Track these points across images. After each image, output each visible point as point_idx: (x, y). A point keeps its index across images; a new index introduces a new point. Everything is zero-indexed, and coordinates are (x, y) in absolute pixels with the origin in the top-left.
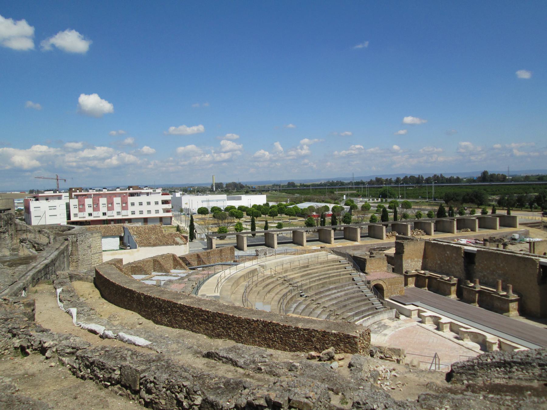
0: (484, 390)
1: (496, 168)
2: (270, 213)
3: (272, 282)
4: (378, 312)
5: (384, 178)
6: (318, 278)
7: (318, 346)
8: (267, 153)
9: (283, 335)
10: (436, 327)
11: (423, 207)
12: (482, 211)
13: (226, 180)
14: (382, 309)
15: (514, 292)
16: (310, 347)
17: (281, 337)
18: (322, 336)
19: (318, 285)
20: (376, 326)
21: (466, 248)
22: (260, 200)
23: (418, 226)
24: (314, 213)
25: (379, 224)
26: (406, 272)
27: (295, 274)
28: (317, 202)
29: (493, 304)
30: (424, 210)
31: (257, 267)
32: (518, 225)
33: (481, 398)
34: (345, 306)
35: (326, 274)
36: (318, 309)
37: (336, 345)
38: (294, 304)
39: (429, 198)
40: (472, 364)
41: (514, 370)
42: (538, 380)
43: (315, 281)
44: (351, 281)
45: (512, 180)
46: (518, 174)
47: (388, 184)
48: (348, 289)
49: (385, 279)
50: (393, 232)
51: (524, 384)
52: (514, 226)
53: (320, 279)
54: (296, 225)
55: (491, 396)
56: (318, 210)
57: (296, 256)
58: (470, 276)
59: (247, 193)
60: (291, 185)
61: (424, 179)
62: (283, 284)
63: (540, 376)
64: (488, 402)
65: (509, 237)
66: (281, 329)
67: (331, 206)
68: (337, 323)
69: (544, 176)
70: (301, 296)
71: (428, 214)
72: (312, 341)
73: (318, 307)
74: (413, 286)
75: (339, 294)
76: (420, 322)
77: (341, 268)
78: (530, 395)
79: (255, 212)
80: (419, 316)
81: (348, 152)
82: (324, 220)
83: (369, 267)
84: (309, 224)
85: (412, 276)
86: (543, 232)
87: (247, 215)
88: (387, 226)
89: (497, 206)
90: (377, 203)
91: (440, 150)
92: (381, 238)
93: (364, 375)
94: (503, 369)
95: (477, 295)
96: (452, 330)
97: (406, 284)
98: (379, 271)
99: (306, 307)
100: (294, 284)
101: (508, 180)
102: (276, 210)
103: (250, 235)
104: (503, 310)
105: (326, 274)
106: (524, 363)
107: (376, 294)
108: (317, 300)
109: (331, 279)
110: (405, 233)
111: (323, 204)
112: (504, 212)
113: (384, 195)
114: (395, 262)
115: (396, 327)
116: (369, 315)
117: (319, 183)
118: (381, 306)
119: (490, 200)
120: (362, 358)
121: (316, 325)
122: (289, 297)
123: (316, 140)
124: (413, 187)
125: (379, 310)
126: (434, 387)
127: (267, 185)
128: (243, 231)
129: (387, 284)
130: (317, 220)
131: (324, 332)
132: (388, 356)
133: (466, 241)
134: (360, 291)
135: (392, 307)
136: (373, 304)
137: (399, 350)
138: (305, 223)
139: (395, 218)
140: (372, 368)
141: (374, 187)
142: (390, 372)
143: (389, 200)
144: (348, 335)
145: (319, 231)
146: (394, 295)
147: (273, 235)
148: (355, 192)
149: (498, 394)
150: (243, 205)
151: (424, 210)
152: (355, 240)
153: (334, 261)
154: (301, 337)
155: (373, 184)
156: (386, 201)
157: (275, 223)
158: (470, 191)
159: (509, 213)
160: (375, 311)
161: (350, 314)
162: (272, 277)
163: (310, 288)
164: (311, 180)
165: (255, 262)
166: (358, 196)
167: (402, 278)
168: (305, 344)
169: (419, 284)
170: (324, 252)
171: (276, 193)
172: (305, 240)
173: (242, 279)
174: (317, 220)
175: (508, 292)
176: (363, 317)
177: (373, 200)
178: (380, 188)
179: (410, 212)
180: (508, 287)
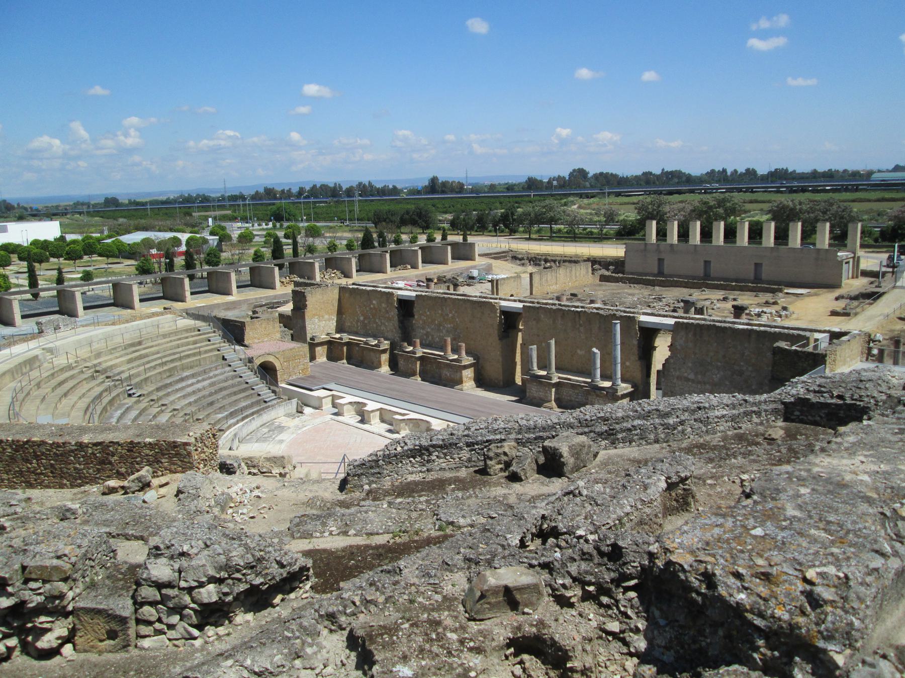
0: (390, 495)
1: (449, 173)
2: (67, 254)
3: (72, 377)
4: (269, 407)
5: (279, 189)
6: (159, 361)
7: (123, 470)
8: (57, 142)
9: (56, 461)
10: (360, 418)
11: (339, 235)
12: (428, 236)
14: (275, 402)
15: (468, 353)
16: (108, 473)
17: (52, 465)
18: (128, 451)
19: (160, 373)
20: (266, 430)
21: (400, 292)
22: (48, 231)
23: (331, 263)
24: (154, 251)
25: (268, 263)
26: (312, 339)
27: (117, 358)
28: (160, 231)
29: (439, 375)
30: (341, 238)
31: (37, 352)
32: (477, 256)
33: (385, 506)
34: (212, 404)
35: (174, 354)
36: (162, 415)
37: (155, 462)
38: (116, 410)
39: (350, 220)
40: (375, 458)
41: (434, 458)
42: (467, 467)
43: (154, 368)
44: (221, 362)
45: (472, 191)
46: (481, 182)
47: (285, 199)
48: (215, 376)
49: (278, 353)
50: (292, 276)
51: (448, 475)
52: (471, 258)
54: (120, 274)
55: (399, 500)
56: (160, 245)
57: (117, 327)
58: (407, 336)
59: (21, 218)
60: (111, 202)
62: (93, 378)
63: (469, 460)
64: (394, 511)
65: (465, 275)
66: (49, 450)
67: (184, 237)
68: (157, 426)
69: (515, 185)
70: (130, 395)
71: (347, 245)
72: (110, 463)
73: (162, 411)
74: (325, 359)
75: (199, 386)
76: (335, 414)
77: (201, 341)
78: (453, 490)
79: (35, 254)
80: (334, 405)
81: (211, 143)
82: (172, 261)
83: (250, 335)
84: (144, 270)
85: (321, 344)
86: (511, 265)
87: (21, 259)
88: (281, 267)
89: (449, 230)
90: (267, 229)
91: (366, 141)
92: (273, 287)
93: (203, 505)
94: (418, 459)
95: (418, 363)
96: (383, 420)
97: (313, 358)
98: (267, 341)
99: (140, 414)
100: (114, 376)
101: (467, 191)
102: (79, 248)
103: (29, 296)
104: (454, 382)
105: (174, 354)
106: (447, 446)
107: (263, 378)
108: (160, 399)
109: (184, 361)
110: (312, 277)
111: (169, 235)
112: (459, 239)
113: (278, 217)
114: (294, 324)
115: (297, 427)
116: (253, 414)
117: (164, 198)
118: (272, 396)
119: (440, 221)
120: (199, 477)
121: (117, 434)
122: (105, 400)
123: (153, 120)
124: (326, 202)
125: (269, 404)
126: (318, 503)
127: (63, 204)
128: (12, 290)
129: (282, 360)
130: (158, 264)
131: (132, 443)
132: (264, 470)
133: (403, 283)
134: (236, 377)
135: (290, 396)
136: (259, 395)
137: (283, 457)
138: (137, 269)
139: (295, 253)
140: (219, 490)
141: (262, 204)
142: (251, 491)
143: (286, 224)
144: (174, 442)
145: (163, 280)
146: (294, 377)
147: (73, 293)
148: (229, 212)
149: (409, 497)
150: (10, 241)
151: (341, 238)
152: (228, 293)
153: (188, 330)
154: (88, 460)
155: (260, 199)
156: (281, 226)
157: (79, 272)
158: (412, 207)
159: (465, 239)
160: (263, 405)
161: (220, 416)
162: (70, 367)
163: (146, 379)
164: (149, 194)
165: (33, 344)
166: (233, 219)
167: (306, 348)
168: (98, 470)
169: (333, 357)
170: (169, 316)
171: (81, 217)
172: (136, 299)
173: (8, 377)
174: (159, 263)
175: (459, 355)
176: (243, 419)
177: (259, 225)
178: (272, 205)
179: (320, 244)
180: (460, 346)
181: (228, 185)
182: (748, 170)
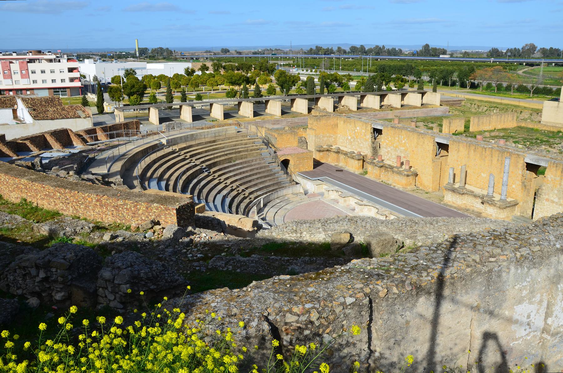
13: (151, 45)
22: (177, 68)
53: (226, 155)
61: (538, 48)
181: (293, 45)
182: (174, 75)
